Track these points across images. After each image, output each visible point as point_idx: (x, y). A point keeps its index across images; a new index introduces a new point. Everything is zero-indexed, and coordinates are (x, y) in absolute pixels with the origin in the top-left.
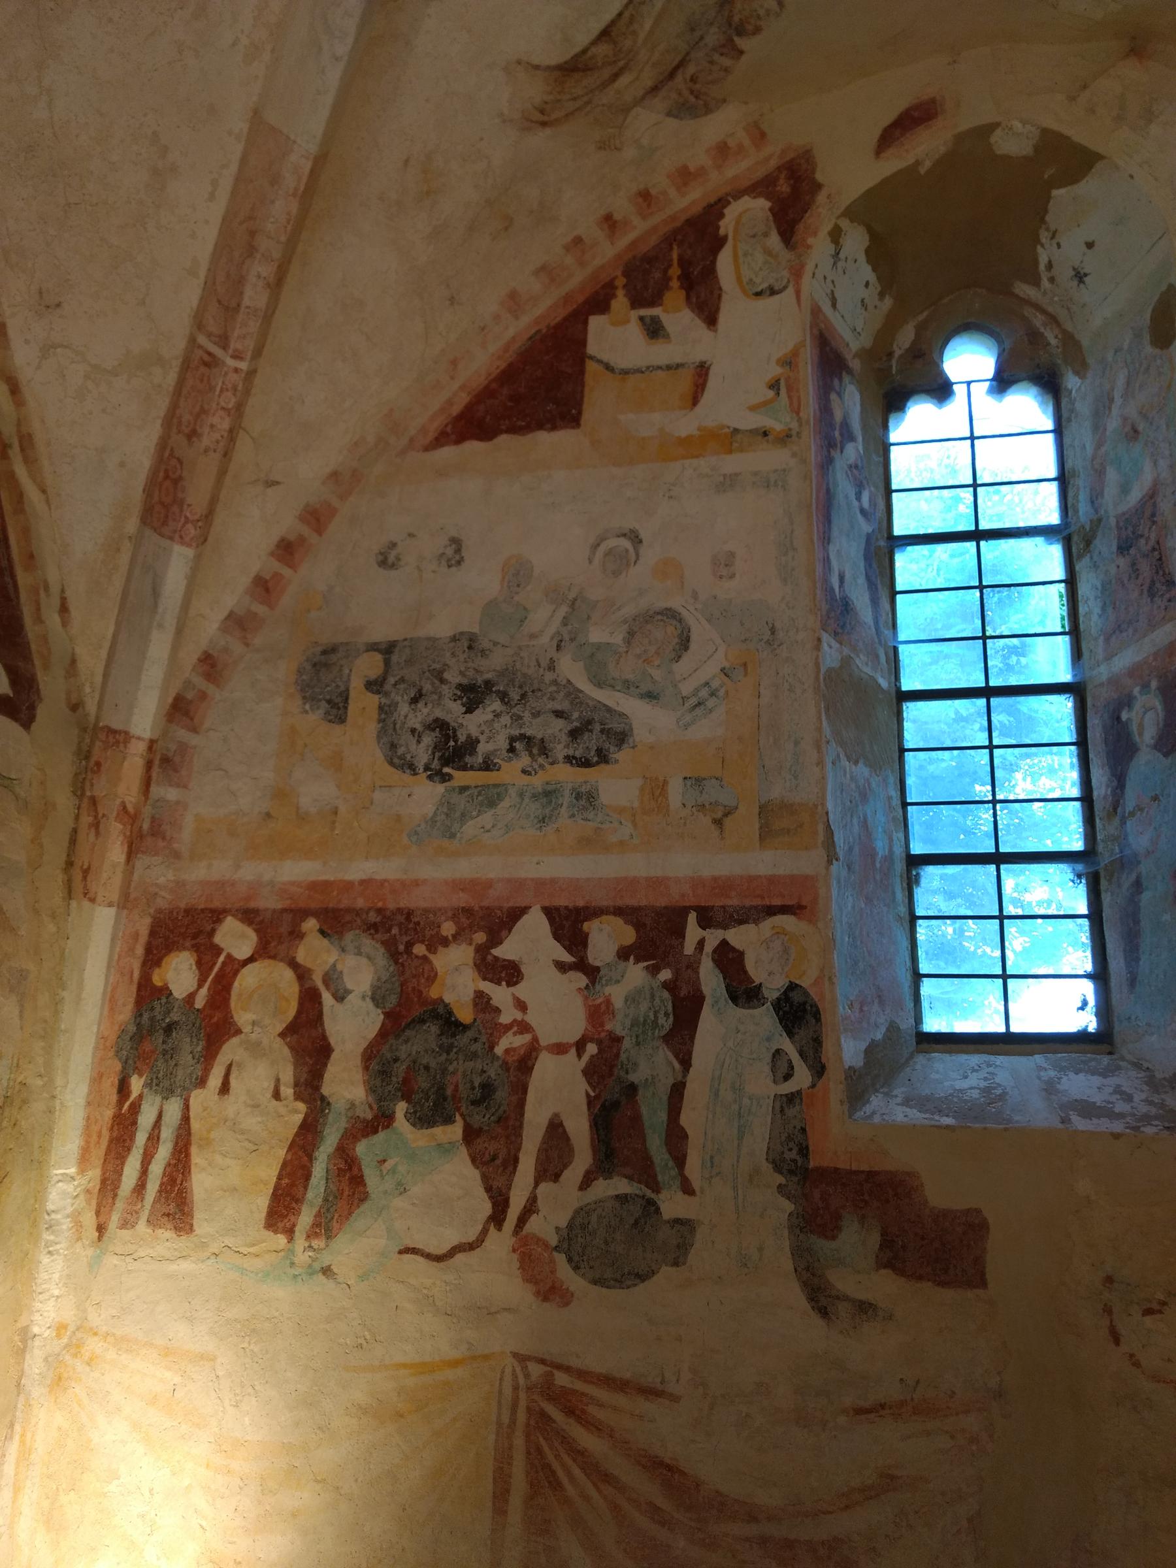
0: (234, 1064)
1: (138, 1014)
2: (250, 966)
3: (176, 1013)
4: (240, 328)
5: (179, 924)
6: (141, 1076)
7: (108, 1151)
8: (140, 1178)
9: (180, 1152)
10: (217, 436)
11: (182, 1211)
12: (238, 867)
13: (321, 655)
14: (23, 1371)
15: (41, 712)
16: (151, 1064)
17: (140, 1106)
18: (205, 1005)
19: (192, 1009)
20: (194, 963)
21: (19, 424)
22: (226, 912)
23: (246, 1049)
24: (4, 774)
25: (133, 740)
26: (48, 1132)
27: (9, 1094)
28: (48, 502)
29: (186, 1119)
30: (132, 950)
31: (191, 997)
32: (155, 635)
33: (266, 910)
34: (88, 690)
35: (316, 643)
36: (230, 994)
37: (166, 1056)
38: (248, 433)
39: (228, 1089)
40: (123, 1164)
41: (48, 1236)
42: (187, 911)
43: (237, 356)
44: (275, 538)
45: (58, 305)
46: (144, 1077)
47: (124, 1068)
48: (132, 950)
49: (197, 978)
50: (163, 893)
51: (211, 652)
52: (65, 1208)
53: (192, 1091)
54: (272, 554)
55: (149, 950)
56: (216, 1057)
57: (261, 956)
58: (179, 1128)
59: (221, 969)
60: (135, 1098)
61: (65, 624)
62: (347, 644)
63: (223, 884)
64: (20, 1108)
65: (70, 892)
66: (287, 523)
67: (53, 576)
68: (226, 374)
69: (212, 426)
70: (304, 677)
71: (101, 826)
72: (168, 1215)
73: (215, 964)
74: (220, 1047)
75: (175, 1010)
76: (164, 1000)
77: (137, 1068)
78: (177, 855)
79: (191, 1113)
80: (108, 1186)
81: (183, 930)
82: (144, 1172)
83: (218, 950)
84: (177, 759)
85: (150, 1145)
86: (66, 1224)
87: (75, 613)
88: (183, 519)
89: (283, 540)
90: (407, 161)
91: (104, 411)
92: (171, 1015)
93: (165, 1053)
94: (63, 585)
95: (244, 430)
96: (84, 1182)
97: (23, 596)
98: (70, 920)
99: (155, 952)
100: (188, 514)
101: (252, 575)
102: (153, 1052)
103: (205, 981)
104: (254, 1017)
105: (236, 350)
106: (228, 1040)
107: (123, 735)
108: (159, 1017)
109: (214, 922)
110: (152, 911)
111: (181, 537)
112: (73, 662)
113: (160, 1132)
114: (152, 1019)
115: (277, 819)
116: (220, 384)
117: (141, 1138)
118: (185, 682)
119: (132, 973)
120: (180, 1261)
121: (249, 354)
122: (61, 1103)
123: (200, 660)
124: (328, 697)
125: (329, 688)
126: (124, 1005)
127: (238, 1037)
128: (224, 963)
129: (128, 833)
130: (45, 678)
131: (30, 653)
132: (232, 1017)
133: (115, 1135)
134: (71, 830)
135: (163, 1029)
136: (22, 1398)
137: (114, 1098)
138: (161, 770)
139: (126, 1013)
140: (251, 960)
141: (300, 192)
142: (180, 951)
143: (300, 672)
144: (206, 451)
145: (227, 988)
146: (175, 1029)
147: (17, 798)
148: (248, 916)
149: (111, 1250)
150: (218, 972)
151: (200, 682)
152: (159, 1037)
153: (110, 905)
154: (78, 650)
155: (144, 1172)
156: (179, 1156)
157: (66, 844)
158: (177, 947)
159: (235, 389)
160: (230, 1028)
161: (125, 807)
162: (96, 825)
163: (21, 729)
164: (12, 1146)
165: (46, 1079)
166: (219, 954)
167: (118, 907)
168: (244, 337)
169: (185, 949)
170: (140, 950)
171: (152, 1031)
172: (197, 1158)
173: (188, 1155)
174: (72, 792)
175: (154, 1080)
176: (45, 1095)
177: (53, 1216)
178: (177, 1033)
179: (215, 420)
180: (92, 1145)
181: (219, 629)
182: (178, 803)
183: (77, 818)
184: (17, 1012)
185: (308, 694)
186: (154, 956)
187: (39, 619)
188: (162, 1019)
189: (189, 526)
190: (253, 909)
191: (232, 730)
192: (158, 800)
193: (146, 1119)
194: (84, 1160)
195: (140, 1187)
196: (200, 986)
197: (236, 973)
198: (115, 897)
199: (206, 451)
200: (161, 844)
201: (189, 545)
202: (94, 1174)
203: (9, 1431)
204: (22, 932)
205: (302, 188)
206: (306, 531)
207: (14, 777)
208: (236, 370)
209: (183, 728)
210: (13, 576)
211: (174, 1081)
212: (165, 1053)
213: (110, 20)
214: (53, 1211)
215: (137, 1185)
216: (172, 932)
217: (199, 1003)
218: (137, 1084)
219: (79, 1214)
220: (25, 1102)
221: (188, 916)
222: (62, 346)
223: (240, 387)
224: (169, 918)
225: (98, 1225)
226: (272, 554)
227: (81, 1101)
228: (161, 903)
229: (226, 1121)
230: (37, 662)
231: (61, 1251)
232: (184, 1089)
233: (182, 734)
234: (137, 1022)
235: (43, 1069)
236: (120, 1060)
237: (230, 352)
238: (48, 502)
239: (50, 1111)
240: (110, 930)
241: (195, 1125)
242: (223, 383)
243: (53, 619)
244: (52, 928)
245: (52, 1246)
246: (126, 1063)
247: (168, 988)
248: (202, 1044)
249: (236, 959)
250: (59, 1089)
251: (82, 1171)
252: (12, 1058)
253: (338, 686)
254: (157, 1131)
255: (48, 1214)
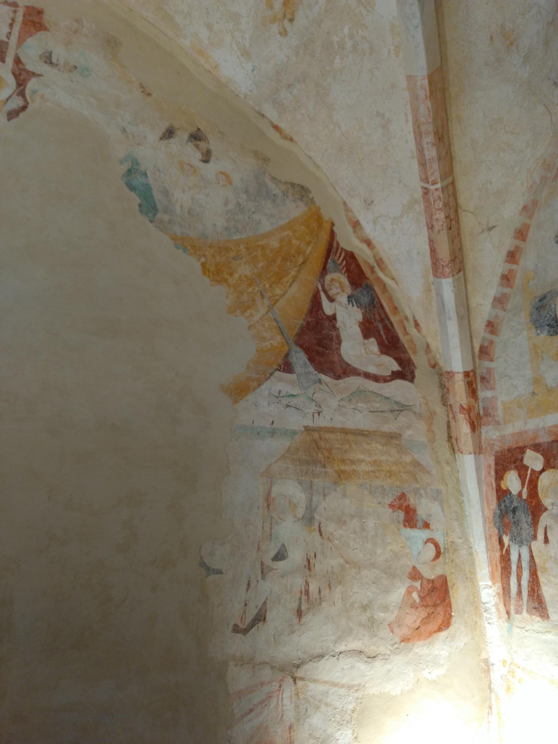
0: (548, 527)
1: (499, 505)
2: (544, 474)
3: (515, 502)
4: (430, 170)
5: (507, 457)
6: (507, 535)
7: (502, 574)
8: (518, 588)
9: (533, 575)
10: (441, 223)
11: (541, 606)
12: (526, 423)
13: (539, 302)
14: (490, 680)
15: (417, 373)
16: (510, 530)
17: (510, 551)
18: (527, 497)
19: (522, 499)
20: (517, 476)
21: (375, 257)
22: (526, 447)
23: (552, 518)
24: (407, 404)
25: (456, 375)
26: (473, 564)
27: (446, 547)
28: (396, 282)
29: (532, 557)
30: (489, 473)
31: (520, 494)
32: (449, 323)
33: (544, 443)
34: (438, 356)
35: (535, 297)
36: (538, 490)
37: (516, 525)
38: (468, 211)
39: (548, 541)
40: (509, 580)
41: (485, 615)
42: (509, 450)
43: (434, 183)
44: (505, 253)
45: (372, 202)
46: (508, 535)
47: (499, 532)
48: (489, 473)
49: (520, 483)
50: (497, 443)
51: (490, 320)
52: (491, 601)
53: (531, 542)
54: (506, 261)
55: (496, 472)
56: (538, 523)
57: (547, 468)
58: (530, 562)
59: (530, 477)
60: (507, 547)
61: (419, 331)
62: (550, 291)
63: (522, 433)
64: (453, 553)
65: (454, 450)
66: (509, 243)
67: (408, 314)
68: (433, 194)
69: (437, 220)
70: (534, 317)
71: (456, 417)
72: (536, 608)
73: (527, 475)
74: (539, 518)
75: (515, 501)
76: (509, 496)
77: (504, 531)
78: (498, 423)
79: (533, 554)
80: (506, 590)
81: (509, 460)
82: (519, 585)
83: (526, 468)
84: (487, 376)
85: (518, 571)
86: (494, 610)
87: (422, 325)
88: (441, 267)
89: (509, 252)
90: (491, 38)
91: (404, 234)
92: (514, 503)
93: (515, 523)
94: (413, 315)
95: (466, 211)
96: (495, 589)
97: (396, 326)
98: (457, 463)
99: (499, 473)
100: (443, 263)
101: (500, 275)
102: (509, 523)
103: (524, 484)
104: (552, 501)
105: (432, 181)
106: (541, 514)
107: (451, 373)
108: (508, 505)
109: (522, 454)
110: (494, 453)
111: (443, 275)
112: (428, 346)
113: (521, 564)
114: (505, 506)
115: (538, 394)
116: (432, 199)
117: (514, 567)
118: (483, 338)
119: (492, 484)
120: (547, 634)
121: (439, 179)
122: (475, 550)
123: (487, 326)
124: (547, 323)
125: (547, 318)
126: (492, 500)
127: (546, 512)
128: (531, 474)
129: (468, 418)
130: (416, 358)
131: (405, 348)
132: (541, 502)
133: (503, 565)
134: (447, 422)
135: (512, 511)
136: (493, 695)
137: (498, 547)
138: (482, 384)
139: (494, 504)
140: (543, 470)
141: (428, 95)
142: (510, 471)
143: (531, 315)
144: (439, 232)
145: (536, 487)
146: (517, 511)
147: (415, 413)
148: (537, 447)
149: (515, 624)
150: (529, 479)
151: (489, 336)
152: (511, 515)
153: (470, 453)
154: (429, 341)
155: (519, 585)
156: (533, 577)
157: (446, 428)
158: (508, 469)
159: (439, 198)
160: (541, 508)
161: (462, 407)
162: (454, 417)
163: (409, 383)
164: (453, 571)
165: (463, 539)
166: (527, 470)
167: (475, 453)
168: (433, 173)
169: (512, 469)
170: (493, 473)
171: (507, 513)
172: (542, 579)
173: (537, 576)
174: (443, 404)
175: (513, 537)
176: (466, 547)
177: (486, 605)
178: (518, 512)
179: (437, 216)
180: (495, 571)
181: (492, 307)
182: (493, 397)
183: (448, 415)
184: (440, 509)
185: (537, 325)
186: (499, 476)
187: (406, 333)
188: (510, 506)
189: (445, 268)
190: (538, 444)
191: (507, 355)
192: (484, 399)
193: (514, 557)
194: (493, 578)
195: (520, 592)
196: (523, 487)
197: (538, 478)
198: (471, 449)
199: (439, 232)
200: (490, 419)
201: (448, 277)
202: (499, 584)
203: (490, 710)
204: (434, 472)
205: (428, 92)
206: (518, 242)
207: (412, 405)
208: (436, 189)
209: (486, 361)
210: (389, 320)
211: (522, 538)
212: (515, 523)
213: (344, 81)
214: (486, 603)
215: (518, 592)
216: (504, 461)
217: (525, 496)
218: (506, 539)
219: (498, 605)
220: (455, 550)
221: (510, 452)
222: (380, 217)
223: (441, 196)
224: (502, 455)
225: (506, 611)
226: (506, 261)
227: (484, 549)
228: (497, 448)
229: (551, 558)
230: (410, 352)
231: (494, 623)
232: (527, 541)
233: (487, 364)
234: (500, 509)
235: (460, 535)
236: (496, 528)
237: (430, 183)
238: (396, 282)
239: (471, 554)
240: (474, 465)
241: (537, 560)
242: (433, 198)
243: (413, 331)
244: (448, 468)
245: (489, 620)
246: (499, 529)
247: (509, 490)
248: (530, 517)
249: (536, 471)
250: (472, 543)
251: (494, 584)
252: (443, 530)
253: (551, 316)
254: (520, 564)
255: (484, 604)
